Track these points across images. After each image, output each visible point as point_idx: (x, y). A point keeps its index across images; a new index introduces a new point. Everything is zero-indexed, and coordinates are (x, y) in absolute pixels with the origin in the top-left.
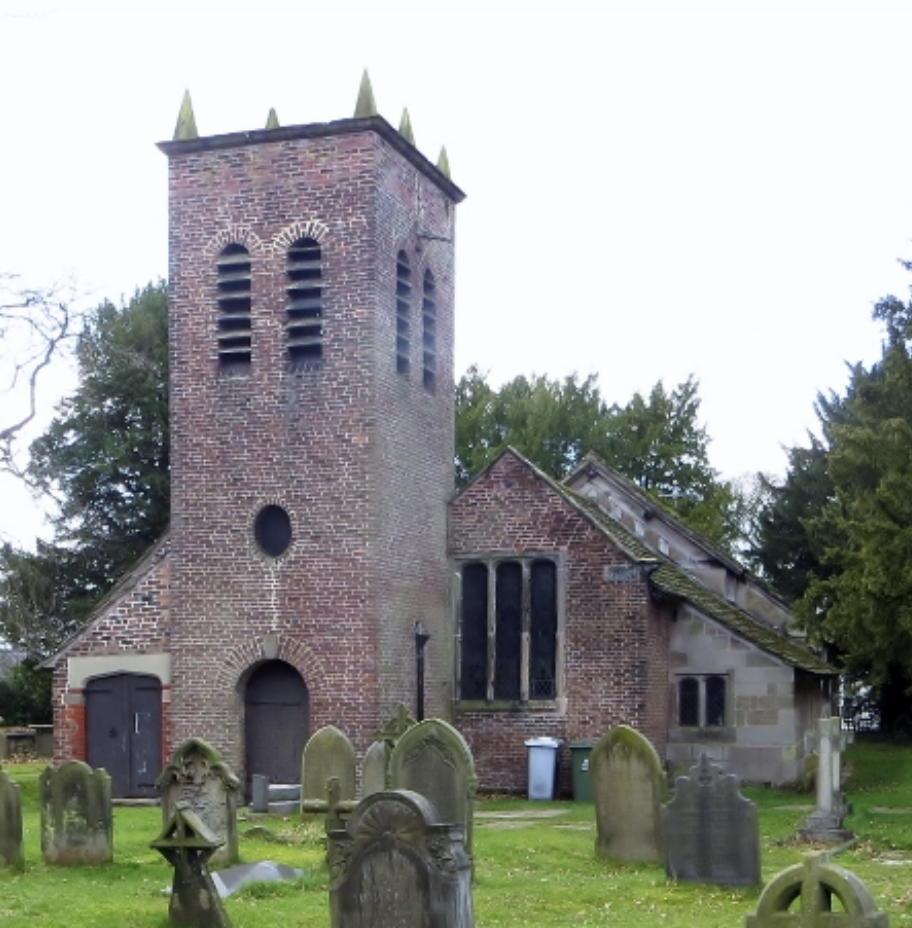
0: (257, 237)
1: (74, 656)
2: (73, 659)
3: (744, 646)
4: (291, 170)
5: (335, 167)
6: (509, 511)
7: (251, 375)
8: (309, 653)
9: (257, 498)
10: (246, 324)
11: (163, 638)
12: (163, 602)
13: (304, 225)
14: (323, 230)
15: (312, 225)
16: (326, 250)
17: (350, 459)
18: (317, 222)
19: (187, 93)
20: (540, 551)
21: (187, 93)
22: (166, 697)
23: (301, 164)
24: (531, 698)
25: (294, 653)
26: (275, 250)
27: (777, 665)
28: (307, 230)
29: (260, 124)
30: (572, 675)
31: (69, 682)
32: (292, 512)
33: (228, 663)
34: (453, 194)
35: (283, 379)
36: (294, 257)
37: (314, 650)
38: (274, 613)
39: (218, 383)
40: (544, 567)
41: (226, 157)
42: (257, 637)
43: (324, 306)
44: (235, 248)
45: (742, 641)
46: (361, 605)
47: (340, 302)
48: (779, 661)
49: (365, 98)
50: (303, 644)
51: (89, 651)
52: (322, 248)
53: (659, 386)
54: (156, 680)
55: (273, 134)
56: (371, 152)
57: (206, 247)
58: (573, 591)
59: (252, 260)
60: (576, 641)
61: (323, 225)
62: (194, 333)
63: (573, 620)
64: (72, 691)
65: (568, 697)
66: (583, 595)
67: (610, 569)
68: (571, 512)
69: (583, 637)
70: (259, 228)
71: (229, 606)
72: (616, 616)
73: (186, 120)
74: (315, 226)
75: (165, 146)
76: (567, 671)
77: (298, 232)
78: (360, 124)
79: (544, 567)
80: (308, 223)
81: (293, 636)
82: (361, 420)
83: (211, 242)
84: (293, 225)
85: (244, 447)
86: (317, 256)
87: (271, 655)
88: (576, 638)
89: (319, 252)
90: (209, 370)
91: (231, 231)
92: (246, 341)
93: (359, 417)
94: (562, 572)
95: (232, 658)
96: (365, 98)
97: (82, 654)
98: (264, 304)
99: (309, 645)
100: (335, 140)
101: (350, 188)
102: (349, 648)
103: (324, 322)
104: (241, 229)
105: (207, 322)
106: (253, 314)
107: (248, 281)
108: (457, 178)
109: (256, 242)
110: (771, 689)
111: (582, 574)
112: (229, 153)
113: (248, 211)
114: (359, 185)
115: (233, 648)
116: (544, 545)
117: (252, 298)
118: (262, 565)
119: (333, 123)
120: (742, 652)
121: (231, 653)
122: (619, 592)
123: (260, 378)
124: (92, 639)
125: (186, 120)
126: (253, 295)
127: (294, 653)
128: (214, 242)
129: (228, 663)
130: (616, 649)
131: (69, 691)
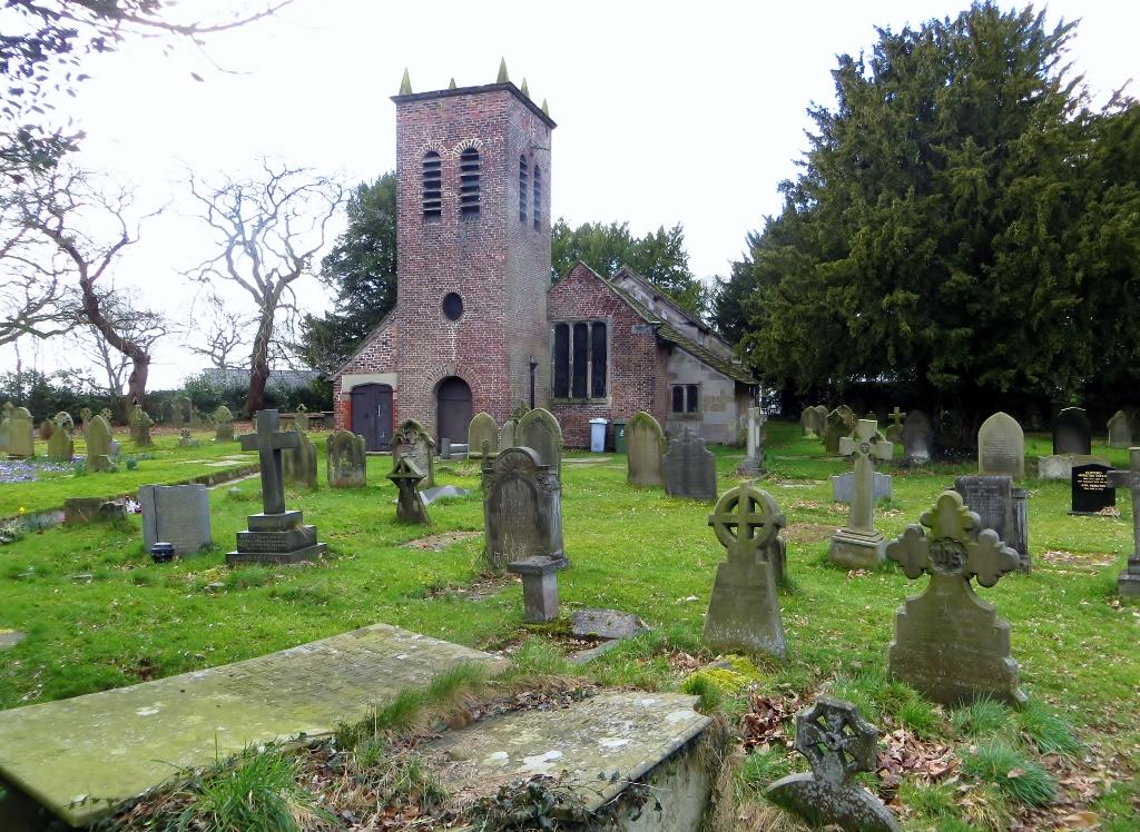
10: (438, 195)
29: (446, 86)
30: (614, 384)
34: (550, 124)
36: (464, 158)
44: (432, 154)
49: (503, 72)
55: (453, 92)
56: (506, 102)
58: (615, 339)
60: (617, 366)
73: (406, 85)
74: (476, 142)
75: (394, 98)
86: (477, 158)
90: (418, 219)
92: (438, 204)
94: (609, 329)
96: (503, 72)
106: (442, 189)
108: (552, 116)
110: (722, 392)
116: (599, 314)
125: (406, 85)
126: (442, 179)
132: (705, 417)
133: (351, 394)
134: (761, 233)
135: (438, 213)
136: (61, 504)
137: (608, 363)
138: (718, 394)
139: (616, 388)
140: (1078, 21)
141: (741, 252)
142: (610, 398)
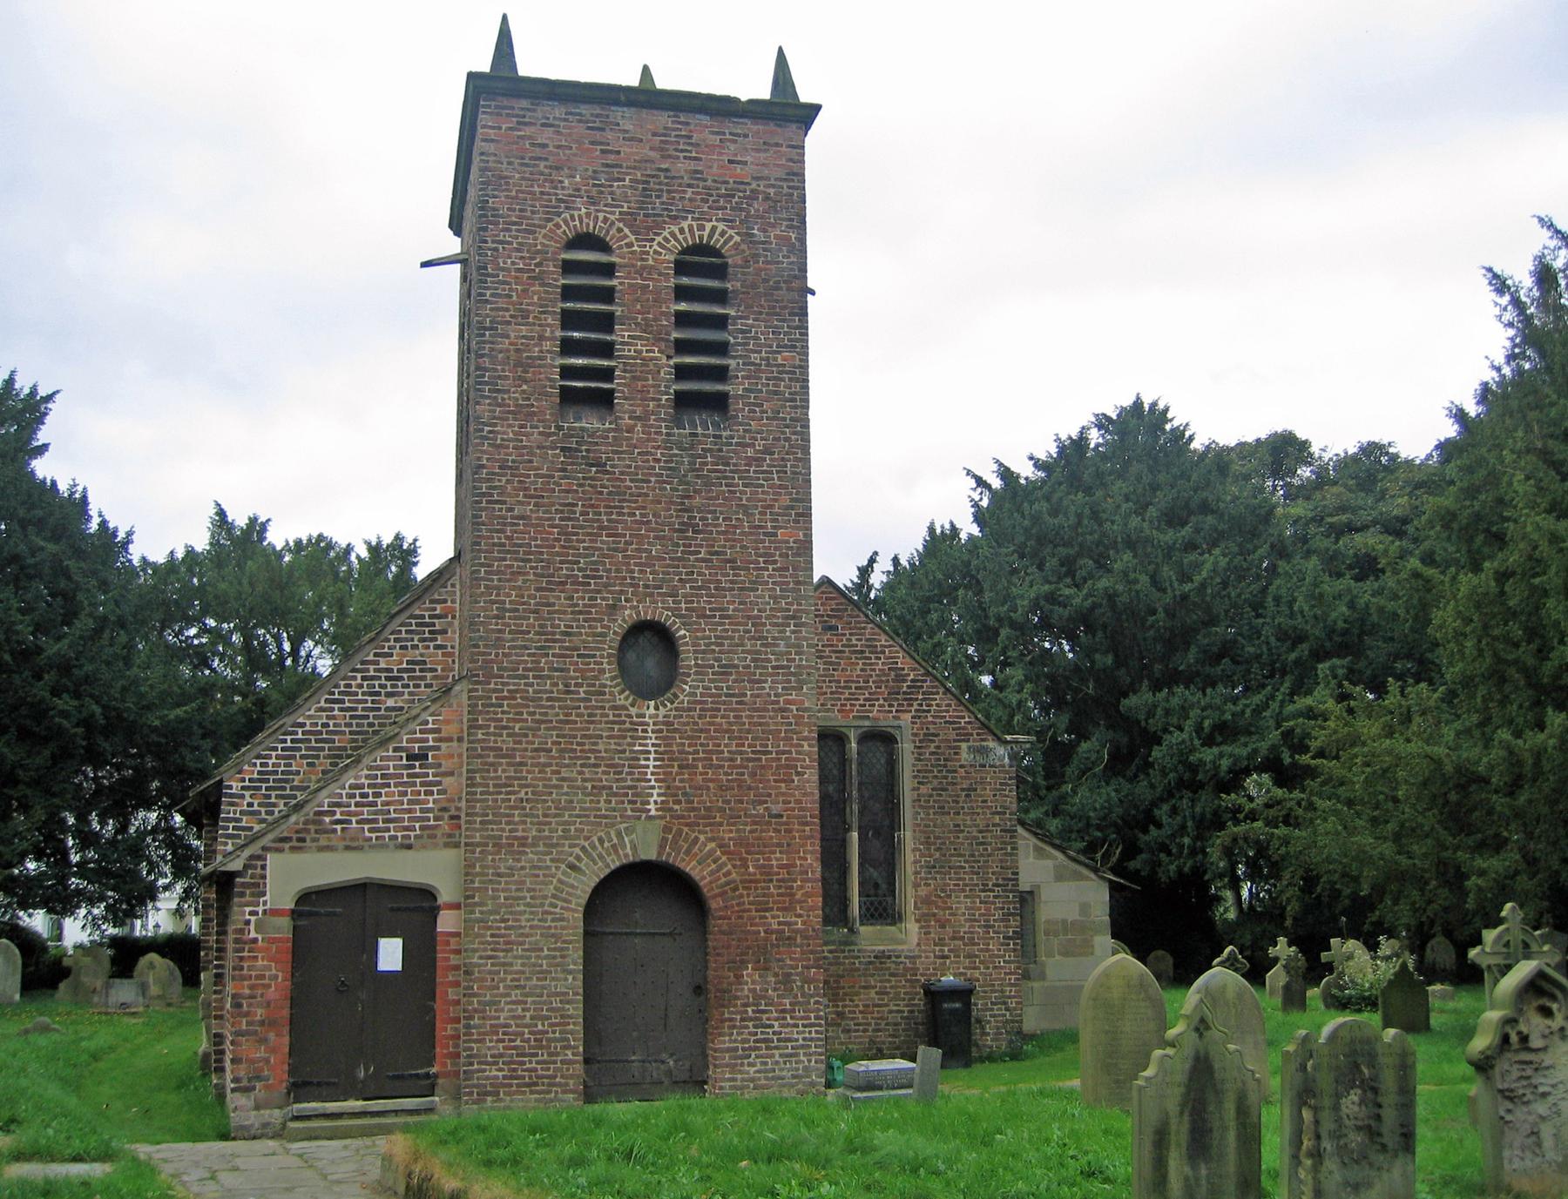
0: (626, 230)
1: (280, 850)
2: (277, 856)
3: (1049, 857)
4: (682, 151)
5: (748, 158)
6: (831, 663)
7: (615, 421)
8: (712, 852)
9: (625, 608)
10: (607, 350)
11: (445, 825)
12: (446, 765)
13: (701, 228)
14: (731, 237)
15: (714, 229)
16: (736, 266)
17: (775, 562)
18: (721, 226)
19: (505, 18)
20: (875, 719)
21: (505, 18)
22: (446, 922)
23: (697, 145)
24: (862, 924)
25: (688, 852)
26: (656, 252)
27: (1087, 878)
28: (706, 233)
30: (923, 891)
31: (267, 897)
32: (682, 632)
33: (572, 867)
35: (668, 434)
36: (681, 268)
37: (720, 846)
38: (653, 787)
39: (560, 428)
40: (882, 739)
41: (580, 114)
42: (623, 826)
43: (732, 341)
44: (584, 240)
45: (1049, 849)
46: (796, 779)
47: (758, 338)
48: (1092, 876)
50: (702, 838)
51: (308, 843)
52: (730, 261)
53: (932, 524)
54: (427, 894)
57: (544, 231)
58: (921, 777)
59: (614, 259)
60: (927, 843)
61: (731, 232)
62: (517, 351)
63: (922, 815)
64: (275, 912)
65: (917, 921)
66: (935, 782)
67: (969, 748)
68: (914, 670)
69: (937, 838)
70: (629, 219)
71: (574, 775)
72: (979, 810)
74: (717, 231)
76: (916, 886)
77: (693, 235)
78: (776, 110)
79: (882, 739)
80: (708, 226)
81: (687, 825)
82: (792, 508)
83: (550, 225)
84: (685, 225)
85: (601, 528)
86: (720, 271)
87: (650, 854)
88: (927, 840)
89: (725, 266)
90: (548, 405)
91: (582, 218)
92: (607, 374)
93: (788, 503)
94: (906, 748)
95: (578, 858)
97: (293, 849)
98: (637, 324)
99: (712, 839)
100: (749, 126)
101: (772, 191)
102: (778, 845)
103: (732, 363)
104: (601, 216)
105: (541, 338)
106: (621, 334)
107: (612, 290)
109: (626, 236)
110: (1085, 908)
111: (932, 753)
112: (586, 110)
113: (612, 193)
114: (786, 190)
115: (582, 842)
116: (880, 715)
117: (618, 314)
118: (633, 711)
119: (751, 102)
120: (1049, 863)
121: (577, 850)
122: (981, 778)
123: (630, 430)
124: (314, 822)
126: (618, 311)
127: (688, 852)
128: (558, 226)
129: (572, 867)
130: (982, 855)
131: (265, 912)
132: (1049, 972)
133: (295, 914)
134: (42, 468)
135: (604, 400)
136: (978, 1068)
137: (908, 837)
138: (1073, 915)
139: (927, 901)
140: (1541, 220)
141: (208, 535)
142: (912, 928)
